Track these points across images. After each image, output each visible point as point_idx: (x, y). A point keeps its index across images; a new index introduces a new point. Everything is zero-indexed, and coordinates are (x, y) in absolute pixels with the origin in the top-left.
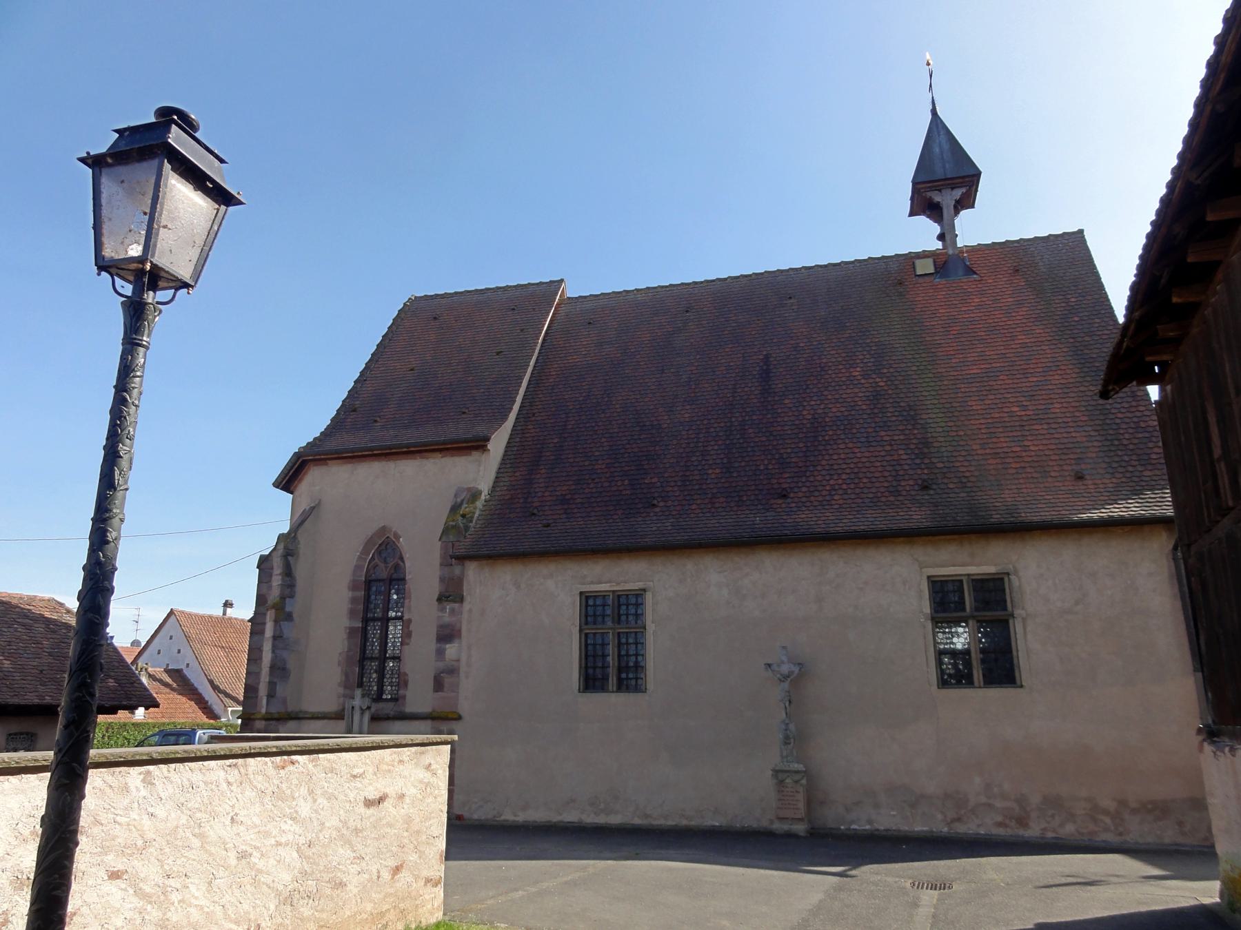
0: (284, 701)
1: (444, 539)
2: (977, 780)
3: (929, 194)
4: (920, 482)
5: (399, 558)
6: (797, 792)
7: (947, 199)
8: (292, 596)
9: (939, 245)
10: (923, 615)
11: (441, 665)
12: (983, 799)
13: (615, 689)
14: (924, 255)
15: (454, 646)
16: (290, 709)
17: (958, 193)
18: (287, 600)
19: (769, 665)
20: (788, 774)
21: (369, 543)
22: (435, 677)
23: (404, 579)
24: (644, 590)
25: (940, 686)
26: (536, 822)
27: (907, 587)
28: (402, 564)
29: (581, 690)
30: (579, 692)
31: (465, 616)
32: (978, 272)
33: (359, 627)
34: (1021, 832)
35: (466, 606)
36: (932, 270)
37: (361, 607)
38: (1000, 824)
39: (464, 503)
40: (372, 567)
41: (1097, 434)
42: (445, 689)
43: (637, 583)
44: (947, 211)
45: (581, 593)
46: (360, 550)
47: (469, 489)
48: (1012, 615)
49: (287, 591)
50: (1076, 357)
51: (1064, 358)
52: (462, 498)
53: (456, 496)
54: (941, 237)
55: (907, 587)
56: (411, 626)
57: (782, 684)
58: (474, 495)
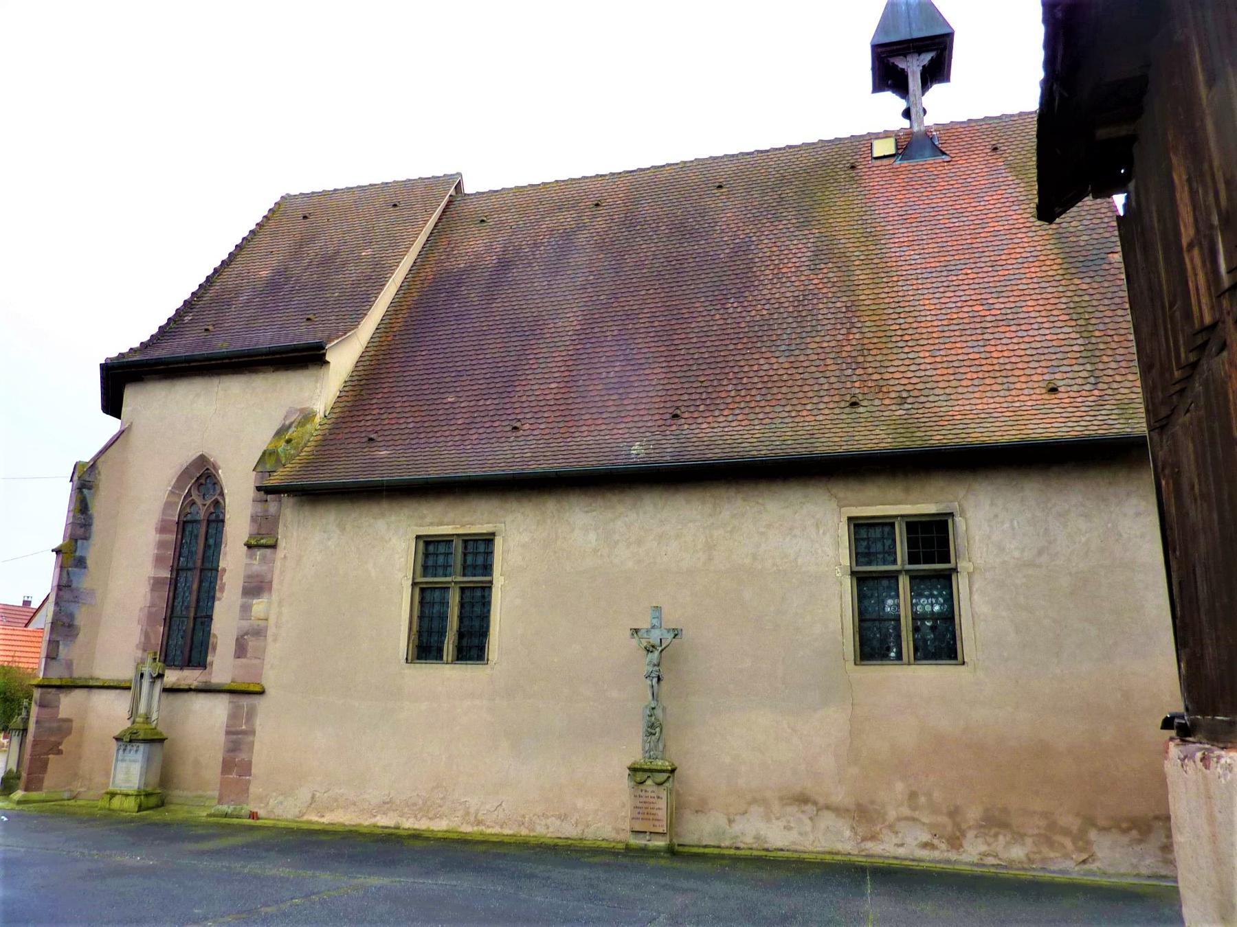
0: (69, 665)
1: (259, 469)
2: (899, 786)
3: (892, 60)
4: (848, 398)
5: (219, 495)
6: (658, 797)
7: (913, 67)
8: (86, 538)
9: (906, 124)
10: (840, 568)
11: (245, 624)
12: (906, 811)
13: (450, 659)
14: (886, 135)
15: (262, 602)
16: (76, 675)
17: (926, 58)
18: (79, 542)
19: (636, 631)
20: (649, 774)
21: (184, 474)
22: (237, 639)
23: (223, 521)
24: (493, 534)
25: (858, 662)
26: (345, 825)
27: (821, 531)
28: (221, 501)
29: (410, 658)
30: (407, 662)
31: (278, 564)
32: (948, 152)
33: (167, 578)
34: (953, 856)
35: (280, 553)
36: (893, 151)
37: (171, 553)
38: (925, 845)
39: (294, 425)
40: (189, 503)
41: (1078, 336)
42: (248, 655)
43: (485, 525)
44: (914, 82)
45: (418, 537)
46: (173, 483)
47: (302, 410)
48: (955, 570)
49: (81, 531)
50: (1059, 246)
51: (1025, 198)
52: (292, 420)
53: (286, 417)
54: (907, 114)
55: (821, 531)
56: (224, 577)
57: (650, 655)
58: (307, 416)
